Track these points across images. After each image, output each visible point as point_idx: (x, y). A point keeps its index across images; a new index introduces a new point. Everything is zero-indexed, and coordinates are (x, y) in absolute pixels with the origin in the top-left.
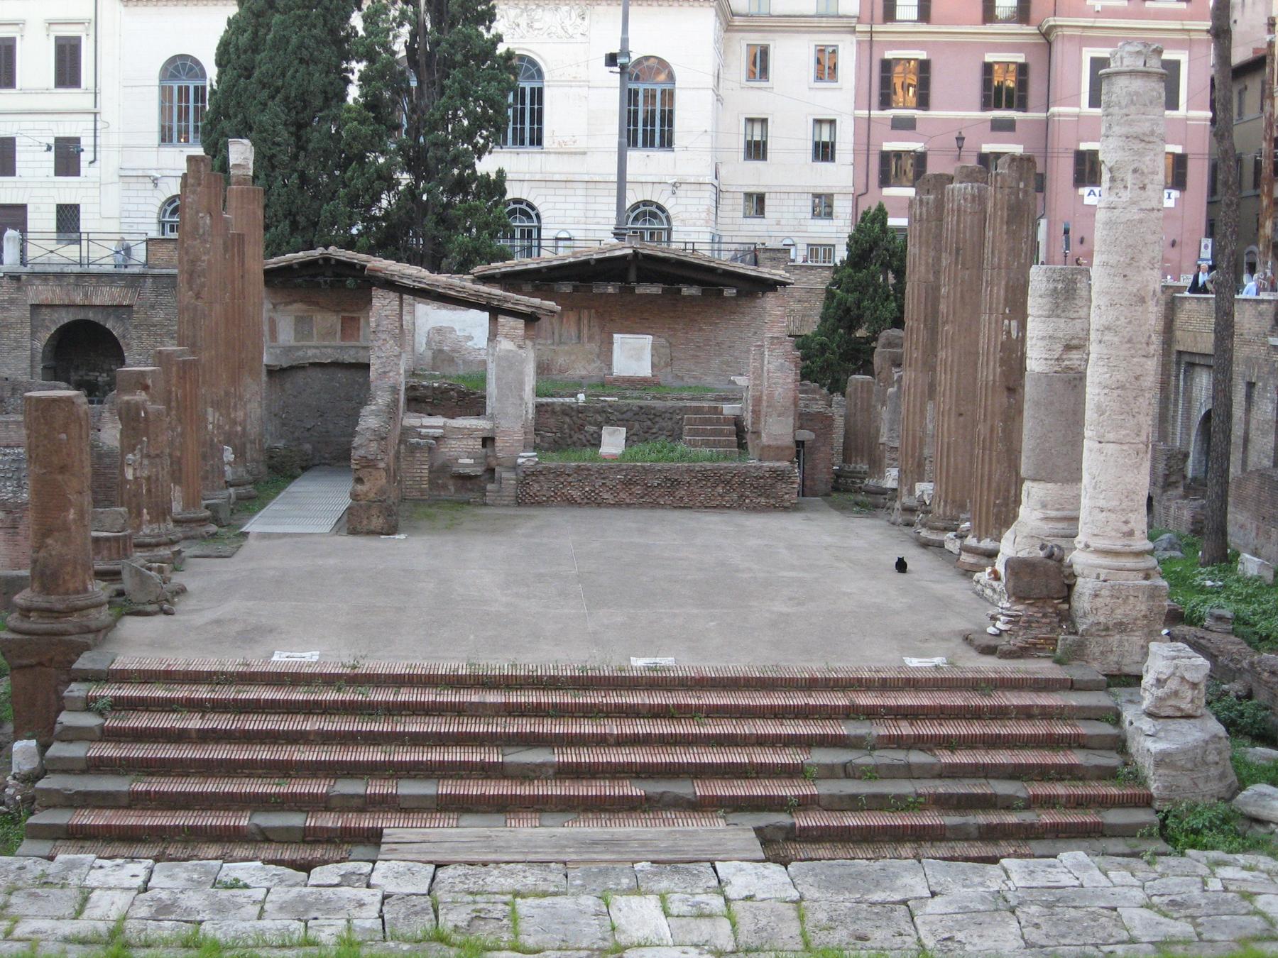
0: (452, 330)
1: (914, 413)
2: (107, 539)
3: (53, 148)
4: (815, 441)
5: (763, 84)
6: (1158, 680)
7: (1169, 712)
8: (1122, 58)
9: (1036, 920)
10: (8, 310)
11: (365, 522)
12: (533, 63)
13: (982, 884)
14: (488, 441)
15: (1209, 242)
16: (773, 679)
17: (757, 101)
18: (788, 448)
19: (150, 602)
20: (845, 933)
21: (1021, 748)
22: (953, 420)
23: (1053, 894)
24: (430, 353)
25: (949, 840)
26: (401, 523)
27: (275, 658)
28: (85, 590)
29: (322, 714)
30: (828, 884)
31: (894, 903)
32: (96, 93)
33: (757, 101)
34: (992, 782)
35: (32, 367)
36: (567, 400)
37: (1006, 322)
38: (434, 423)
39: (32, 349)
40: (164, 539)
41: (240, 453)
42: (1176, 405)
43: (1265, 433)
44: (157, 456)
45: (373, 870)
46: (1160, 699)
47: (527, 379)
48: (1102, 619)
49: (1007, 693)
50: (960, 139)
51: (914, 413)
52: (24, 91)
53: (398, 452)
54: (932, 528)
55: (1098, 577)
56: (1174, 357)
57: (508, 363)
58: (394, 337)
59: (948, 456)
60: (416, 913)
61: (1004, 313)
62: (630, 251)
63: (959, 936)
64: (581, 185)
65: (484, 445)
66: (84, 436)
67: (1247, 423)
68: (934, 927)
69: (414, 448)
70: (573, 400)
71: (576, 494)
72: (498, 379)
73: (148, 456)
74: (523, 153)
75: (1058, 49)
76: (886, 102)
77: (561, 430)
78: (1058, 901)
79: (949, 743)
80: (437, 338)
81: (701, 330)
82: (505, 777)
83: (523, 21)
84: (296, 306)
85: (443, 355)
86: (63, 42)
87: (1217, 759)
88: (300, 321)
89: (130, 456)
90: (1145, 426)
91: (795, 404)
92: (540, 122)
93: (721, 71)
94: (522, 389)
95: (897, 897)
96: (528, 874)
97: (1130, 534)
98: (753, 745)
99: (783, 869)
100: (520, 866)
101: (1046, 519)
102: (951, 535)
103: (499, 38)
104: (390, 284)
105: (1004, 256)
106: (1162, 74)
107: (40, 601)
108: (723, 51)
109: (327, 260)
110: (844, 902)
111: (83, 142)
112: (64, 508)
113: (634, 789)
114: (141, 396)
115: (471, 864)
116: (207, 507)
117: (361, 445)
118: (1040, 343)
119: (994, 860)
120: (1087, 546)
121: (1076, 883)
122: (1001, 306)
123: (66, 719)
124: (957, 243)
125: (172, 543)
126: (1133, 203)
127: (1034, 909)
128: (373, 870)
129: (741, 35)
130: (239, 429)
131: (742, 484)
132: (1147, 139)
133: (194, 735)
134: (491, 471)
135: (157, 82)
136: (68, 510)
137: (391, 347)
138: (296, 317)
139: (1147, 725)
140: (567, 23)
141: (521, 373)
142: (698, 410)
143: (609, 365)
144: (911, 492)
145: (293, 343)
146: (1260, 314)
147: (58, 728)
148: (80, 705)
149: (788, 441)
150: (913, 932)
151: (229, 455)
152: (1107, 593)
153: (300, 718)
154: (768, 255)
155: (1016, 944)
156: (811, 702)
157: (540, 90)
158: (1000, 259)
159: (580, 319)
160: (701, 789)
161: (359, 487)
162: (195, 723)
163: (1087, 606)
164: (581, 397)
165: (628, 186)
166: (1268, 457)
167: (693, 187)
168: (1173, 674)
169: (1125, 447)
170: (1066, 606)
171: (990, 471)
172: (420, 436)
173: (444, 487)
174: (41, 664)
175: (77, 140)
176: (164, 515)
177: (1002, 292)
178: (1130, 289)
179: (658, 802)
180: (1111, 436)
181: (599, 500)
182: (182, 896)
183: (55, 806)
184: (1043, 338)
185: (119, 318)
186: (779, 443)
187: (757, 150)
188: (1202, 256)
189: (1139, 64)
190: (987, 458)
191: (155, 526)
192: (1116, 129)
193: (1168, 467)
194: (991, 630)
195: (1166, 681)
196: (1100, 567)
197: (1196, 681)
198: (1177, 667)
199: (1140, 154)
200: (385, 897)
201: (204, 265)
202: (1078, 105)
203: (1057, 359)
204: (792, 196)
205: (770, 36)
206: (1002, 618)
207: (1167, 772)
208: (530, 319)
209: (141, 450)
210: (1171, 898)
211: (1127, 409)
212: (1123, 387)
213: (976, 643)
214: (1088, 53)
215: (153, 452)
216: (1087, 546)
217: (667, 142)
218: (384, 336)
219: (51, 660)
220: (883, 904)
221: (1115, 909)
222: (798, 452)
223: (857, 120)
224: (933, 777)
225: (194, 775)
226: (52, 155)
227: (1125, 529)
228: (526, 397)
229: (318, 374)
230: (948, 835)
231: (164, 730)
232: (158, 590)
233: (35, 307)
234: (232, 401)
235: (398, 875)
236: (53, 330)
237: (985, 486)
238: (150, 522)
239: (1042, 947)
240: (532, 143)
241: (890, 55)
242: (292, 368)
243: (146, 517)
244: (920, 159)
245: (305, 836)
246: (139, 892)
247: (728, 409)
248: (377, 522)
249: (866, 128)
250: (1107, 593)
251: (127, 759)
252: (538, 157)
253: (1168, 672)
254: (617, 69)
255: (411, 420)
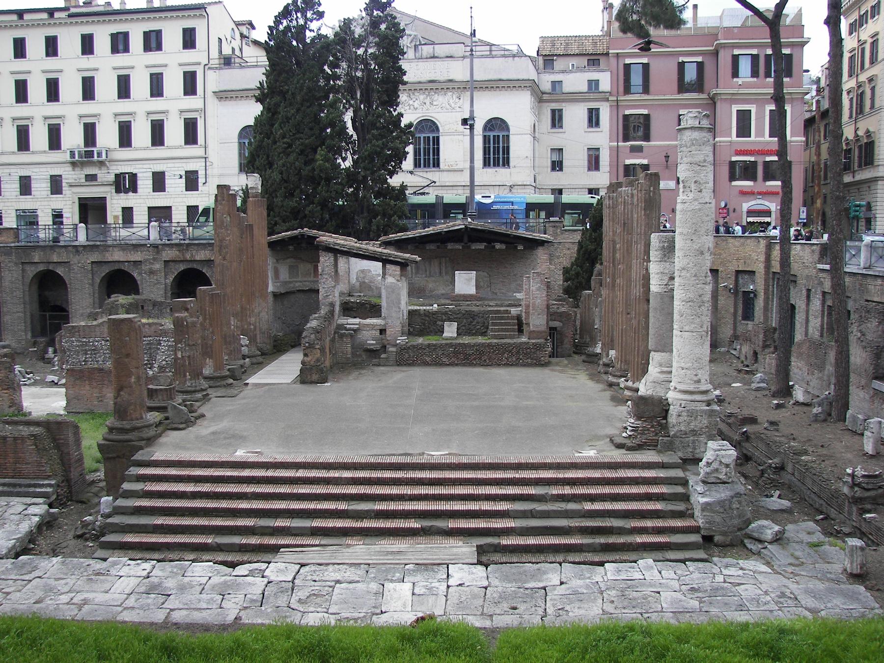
0: (370, 271)
1: (608, 313)
2: (161, 390)
3: (184, 177)
4: (562, 328)
5: (560, 130)
6: (708, 463)
7: (713, 480)
8: (687, 120)
9: (613, 599)
10: (153, 264)
11: (309, 377)
12: (434, 123)
13: (589, 578)
14: (382, 331)
15: (805, 209)
16: (498, 463)
17: (556, 139)
18: (544, 332)
19: (182, 423)
20: (505, 605)
21: (631, 500)
22: (624, 317)
23: (626, 584)
24: (358, 284)
25: (585, 552)
26: (329, 377)
27: (237, 453)
28: (142, 418)
29: (256, 483)
30: (506, 578)
31: (539, 588)
32: (205, 147)
33: (556, 139)
34: (612, 519)
35: (165, 293)
36: (428, 308)
37: (645, 264)
38: (353, 322)
39: (165, 284)
40: (198, 388)
41: (253, 339)
42: (773, 301)
43: (816, 317)
44: (194, 345)
45: (267, 567)
46: (707, 473)
47: (402, 297)
48: (683, 428)
49: (626, 471)
50: (667, 157)
51: (608, 313)
52: (169, 148)
53: (334, 337)
54: (614, 376)
55: (681, 405)
56: (771, 276)
57: (392, 289)
58: (331, 277)
59: (622, 337)
60: (282, 592)
61: (644, 259)
62: (463, 227)
63: (568, 608)
64: (460, 188)
65: (381, 334)
66: (139, 338)
67: (807, 312)
68: (555, 602)
69: (342, 336)
70: (431, 308)
71: (428, 359)
72: (387, 298)
73: (189, 345)
74: (430, 171)
75: (718, 105)
76: (626, 138)
77: (424, 324)
78: (628, 588)
79: (592, 498)
80: (362, 275)
81: (505, 267)
82: (349, 518)
83: (428, 101)
84: (288, 260)
85: (364, 286)
86: (188, 121)
87: (738, 506)
88: (291, 268)
89: (179, 345)
90: (706, 322)
91: (548, 306)
92: (438, 155)
93: (536, 124)
94: (400, 303)
95: (541, 585)
96: (348, 570)
97: (699, 381)
98: (483, 500)
99: (485, 569)
100: (345, 566)
101: (662, 372)
102: (623, 379)
103: (401, 115)
104: (329, 249)
105: (643, 227)
106: (710, 128)
107: (118, 424)
108: (538, 114)
109: (302, 235)
110: (511, 587)
111: (200, 173)
112: (129, 375)
113: (414, 524)
114: (185, 314)
115: (320, 565)
116: (229, 370)
117: (306, 336)
118: (656, 276)
119: (601, 564)
120: (675, 388)
121: (642, 577)
122: (642, 255)
123: (126, 486)
124: (624, 220)
125: (202, 390)
126: (696, 200)
127: (613, 593)
128: (267, 567)
129: (547, 104)
130: (252, 327)
131: (518, 352)
132: (701, 164)
133: (189, 494)
134: (384, 347)
135: (237, 140)
136: (131, 377)
137: (330, 282)
138: (289, 266)
139: (700, 488)
140: (451, 101)
141: (399, 294)
142: (498, 312)
143: (454, 289)
144: (608, 355)
145: (288, 280)
146: (813, 251)
147: (121, 490)
148: (134, 479)
149: (544, 328)
150: (543, 605)
151: (244, 341)
152: (685, 414)
153: (245, 485)
154: (551, 224)
155: (597, 612)
156: (517, 476)
157: (438, 138)
158: (641, 229)
159: (440, 263)
160: (452, 524)
161: (306, 358)
162: (190, 488)
163: (674, 421)
164: (435, 305)
165: (476, 188)
166: (818, 330)
167: (521, 187)
168: (716, 459)
169: (694, 334)
170: (665, 421)
171: (638, 346)
172: (346, 329)
173: (360, 356)
174: (118, 457)
175: (197, 172)
176: (198, 376)
177: (643, 247)
178: (695, 247)
179: (428, 531)
180: (687, 328)
181: (441, 362)
182: (165, 581)
183: (116, 532)
184: (658, 273)
185: (209, 267)
186: (540, 329)
187: (557, 166)
188: (801, 217)
189: (696, 124)
190: (636, 338)
191: (193, 381)
192: (685, 159)
193: (765, 336)
194: (624, 435)
195: (711, 463)
196: (682, 400)
197: (728, 463)
198: (717, 456)
199: (699, 173)
200: (269, 582)
201: (227, 242)
202: (731, 137)
203: (666, 285)
204: (577, 190)
205: (564, 104)
206: (629, 428)
207: (708, 514)
208: (403, 265)
209: (185, 342)
210: (692, 586)
211: (695, 313)
212: (692, 301)
213: (615, 442)
214: (735, 108)
215: (191, 343)
216: (675, 388)
217: (506, 163)
218: (326, 277)
219: (124, 454)
220: (532, 589)
221: (659, 593)
222: (550, 333)
223: (611, 148)
224: (580, 517)
225: (188, 516)
226: (183, 180)
227: (695, 379)
228: (402, 308)
229: (302, 296)
230: (584, 549)
231: (174, 492)
232: (186, 417)
233: (166, 262)
234: (248, 312)
235: (280, 571)
236: (176, 273)
237: (636, 353)
238: (191, 379)
239: (611, 614)
240: (434, 166)
241: (627, 112)
242: (287, 293)
243: (189, 377)
244: (645, 167)
245: (240, 548)
246: (145, 578)
247: (514, 311)
248: (315, 377)
249: (616, 153)
250: (685, 414)
251: (153, 507)
252: (437, 173)
253: (712, 458)
254: (468, 127)
255: (343, 321)
